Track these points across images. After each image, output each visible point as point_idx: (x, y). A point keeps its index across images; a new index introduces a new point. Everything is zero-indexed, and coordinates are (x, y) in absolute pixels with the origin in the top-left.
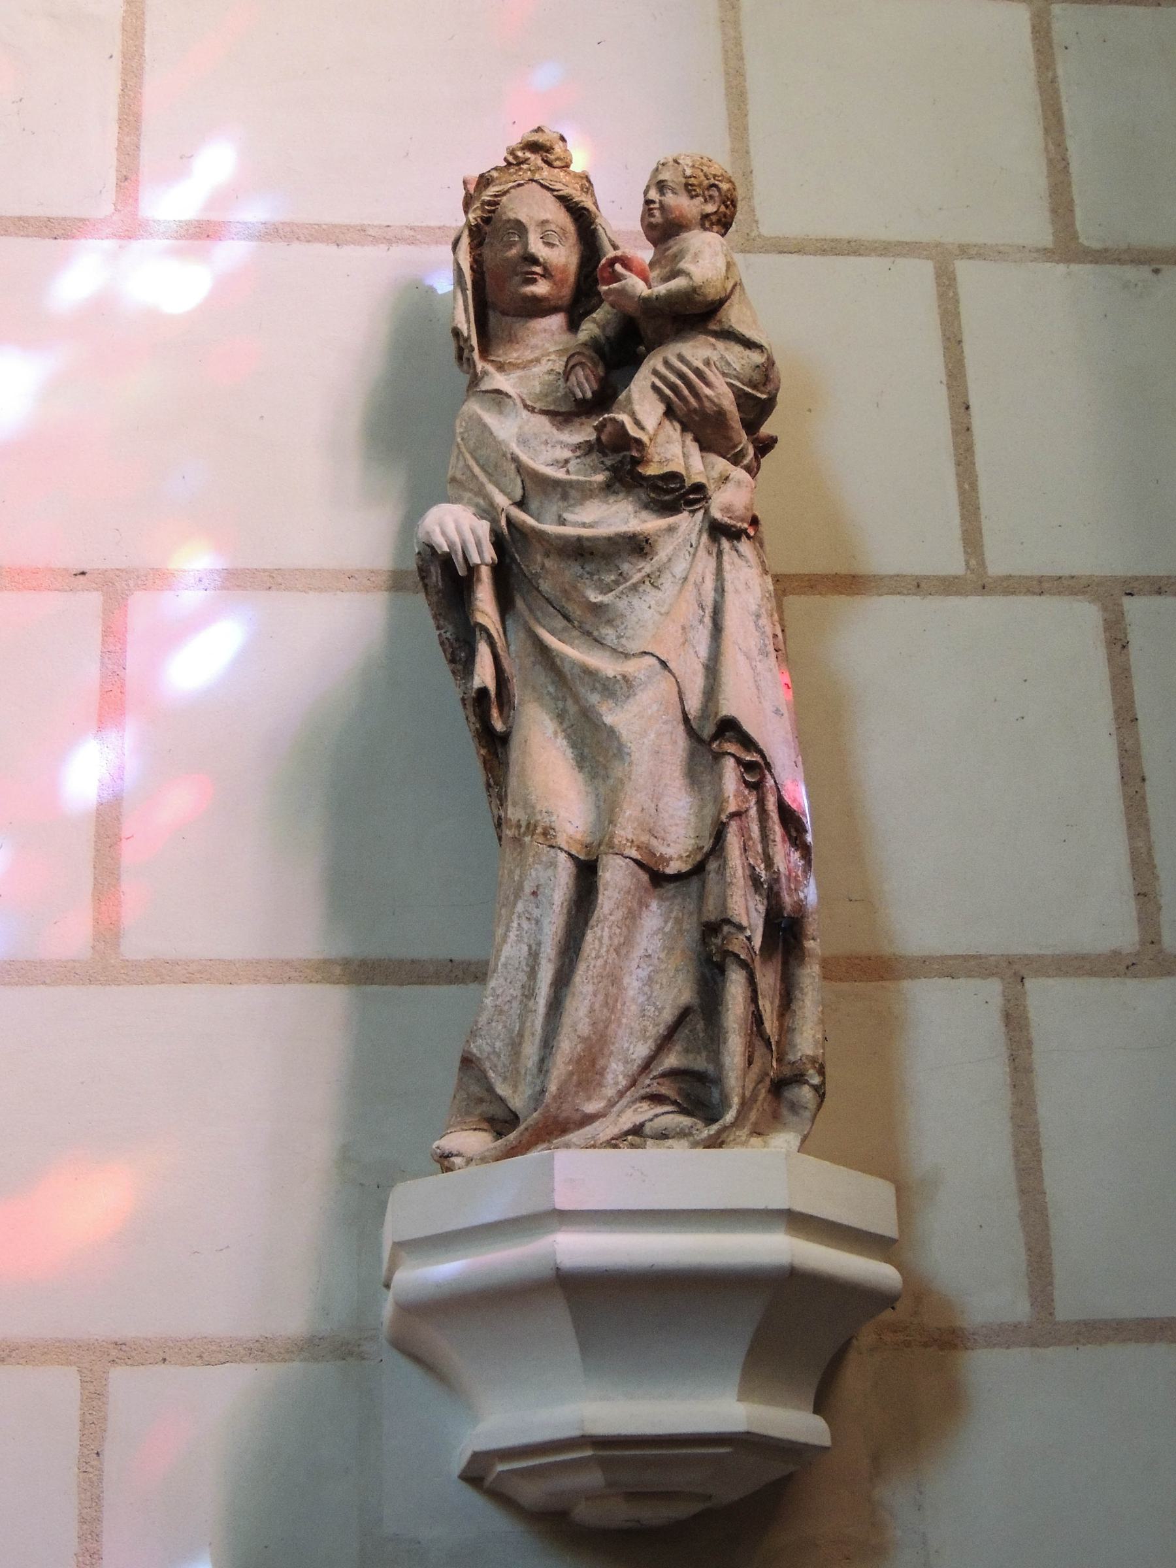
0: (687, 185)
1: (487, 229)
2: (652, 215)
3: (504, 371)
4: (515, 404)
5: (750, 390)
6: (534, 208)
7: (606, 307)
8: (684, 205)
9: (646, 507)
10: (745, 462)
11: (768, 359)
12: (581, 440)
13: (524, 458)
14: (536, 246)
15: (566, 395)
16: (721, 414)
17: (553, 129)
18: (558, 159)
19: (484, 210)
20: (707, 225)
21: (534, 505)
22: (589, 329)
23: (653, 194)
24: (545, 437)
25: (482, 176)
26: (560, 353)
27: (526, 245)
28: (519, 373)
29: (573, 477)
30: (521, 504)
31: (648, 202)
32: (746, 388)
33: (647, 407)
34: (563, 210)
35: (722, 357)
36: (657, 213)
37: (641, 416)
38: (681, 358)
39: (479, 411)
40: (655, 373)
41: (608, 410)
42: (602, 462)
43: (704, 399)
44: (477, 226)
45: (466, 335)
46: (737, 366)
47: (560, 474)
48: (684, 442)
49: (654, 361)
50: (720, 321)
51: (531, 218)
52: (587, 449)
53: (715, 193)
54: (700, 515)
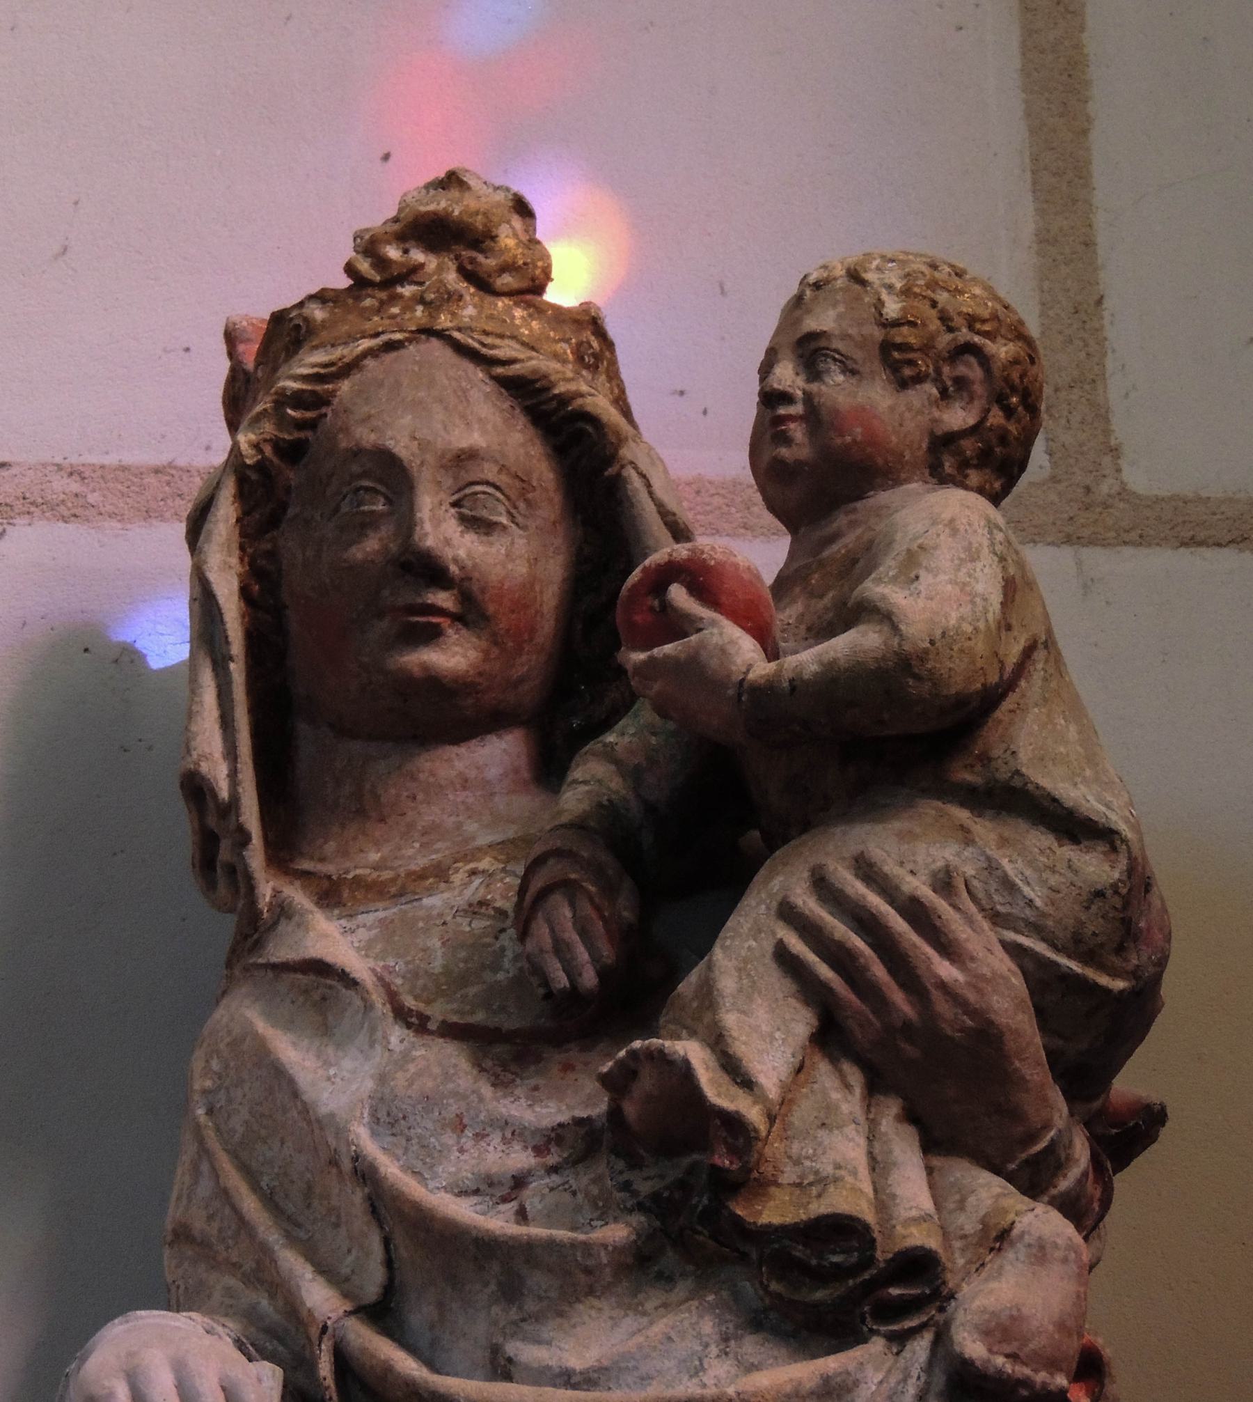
0: (886, 347)
1: (293, 476)
2: (786, 440)
3: (340, 904)
4: (368, 1007)
5: (1075, 966)
6: (436, 415)
7: (644, 713)
8: (884, 409)
9: (757, 1323)
10: (1065, 1184)
11: (1131, 871)
12: (564, 1118)
13: (391, 1169)
14: (440, 530)
15: (518, 981)
16: (986, 1037)
17: (493, 174)
18: (504, 269)
19: (282, 421)
20: (948, 466)
21: (419, 1315)
22: (592, 779)
23: (787, 375)
24: (453, 1108)
25: (278, 318)
26: (505, 849)
27: (407, 524)
28: (381, 912)
29: (537, 1231)
30: (382, 1313)
31: (771, 399)
32: (1063, 961)
33: (761, 1015)
34: (521, 420)
35: (991, 867)
36: (797, 431)
37: (744, 1048)
38: (867, 870)
39: (261, 1026)
40: (788, 913)
41: (650, 1030)
42: (626, 1186)
43: (936, 995)
44: (261, 467)
45: (224, 794)
46: (1035, 893)
47: (498, 1222)
48: (873, 1124)
49: (786, 880)
50: (985, 759)
51: (424, 446)
52: (577, 1144)
53: (971, 370)
54: (920, 1348)
